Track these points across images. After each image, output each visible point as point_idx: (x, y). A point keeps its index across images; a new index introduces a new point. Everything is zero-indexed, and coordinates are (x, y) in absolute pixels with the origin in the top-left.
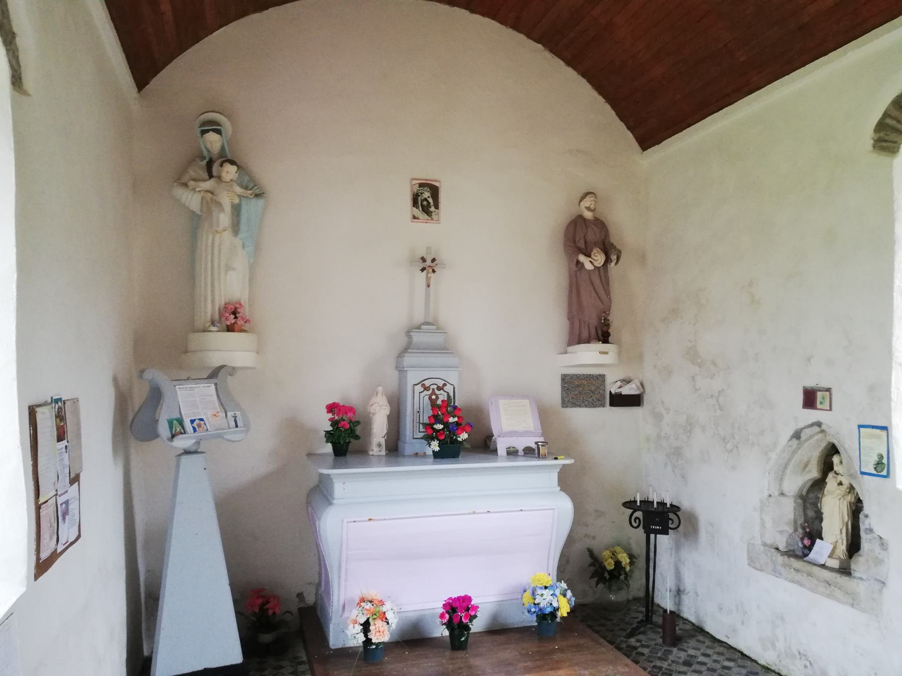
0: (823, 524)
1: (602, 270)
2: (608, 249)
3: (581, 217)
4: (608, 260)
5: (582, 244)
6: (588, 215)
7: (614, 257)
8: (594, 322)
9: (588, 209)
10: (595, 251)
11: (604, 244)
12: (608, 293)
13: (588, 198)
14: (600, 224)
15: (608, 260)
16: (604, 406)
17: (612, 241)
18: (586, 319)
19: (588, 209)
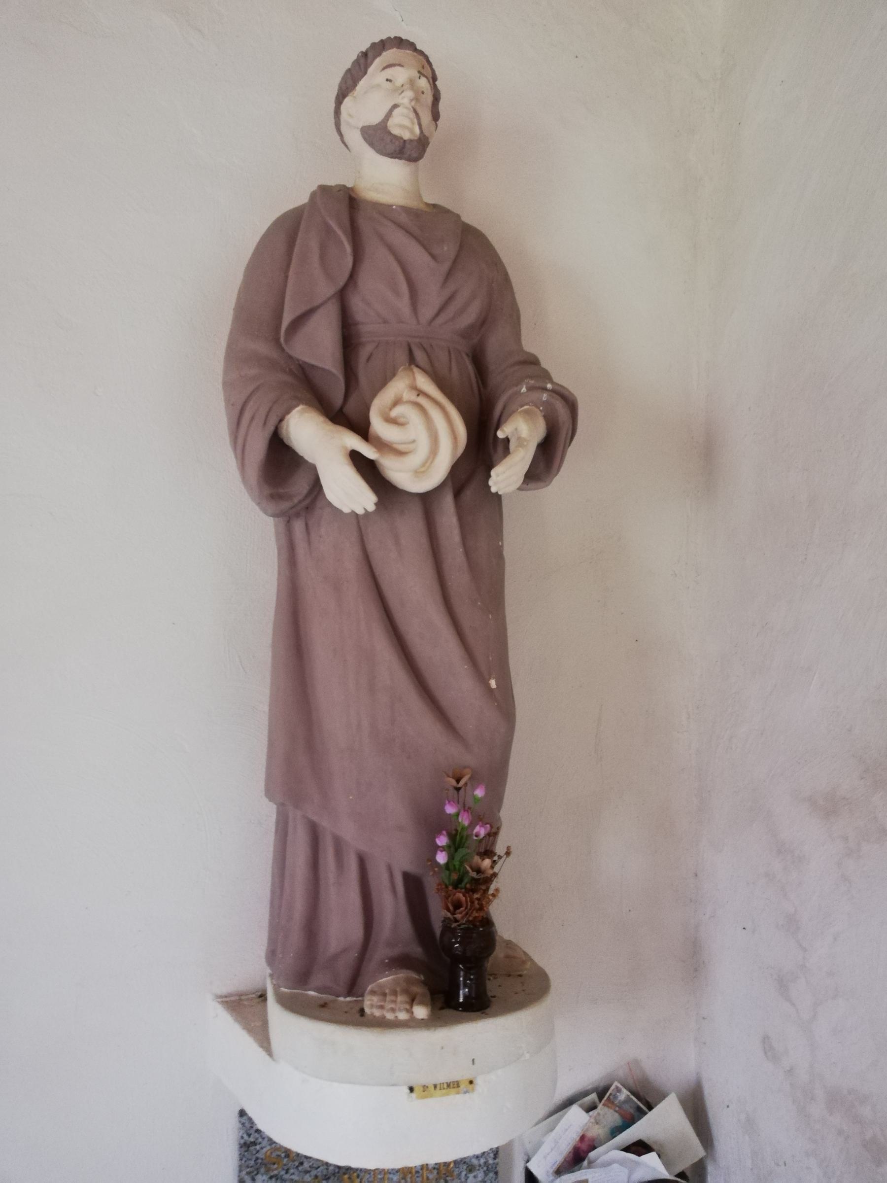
0: (377, 41)
1: (447, 508)
2: (484, 382)
3: (346, 206)
4: (482, 447)
5: (319, 346)
6: (385, 181)
7: (522, 431)
8: (395, 852)
9: (379, 138)
10: (398, 386)
11: (478, 359)
12: (489, 660)
13: (375, 75)
14: (466, 248)
15: (482, 447)
16: (646, 1114)
17: (530, 344)
18: (349, 831)
19: (379, 138)
